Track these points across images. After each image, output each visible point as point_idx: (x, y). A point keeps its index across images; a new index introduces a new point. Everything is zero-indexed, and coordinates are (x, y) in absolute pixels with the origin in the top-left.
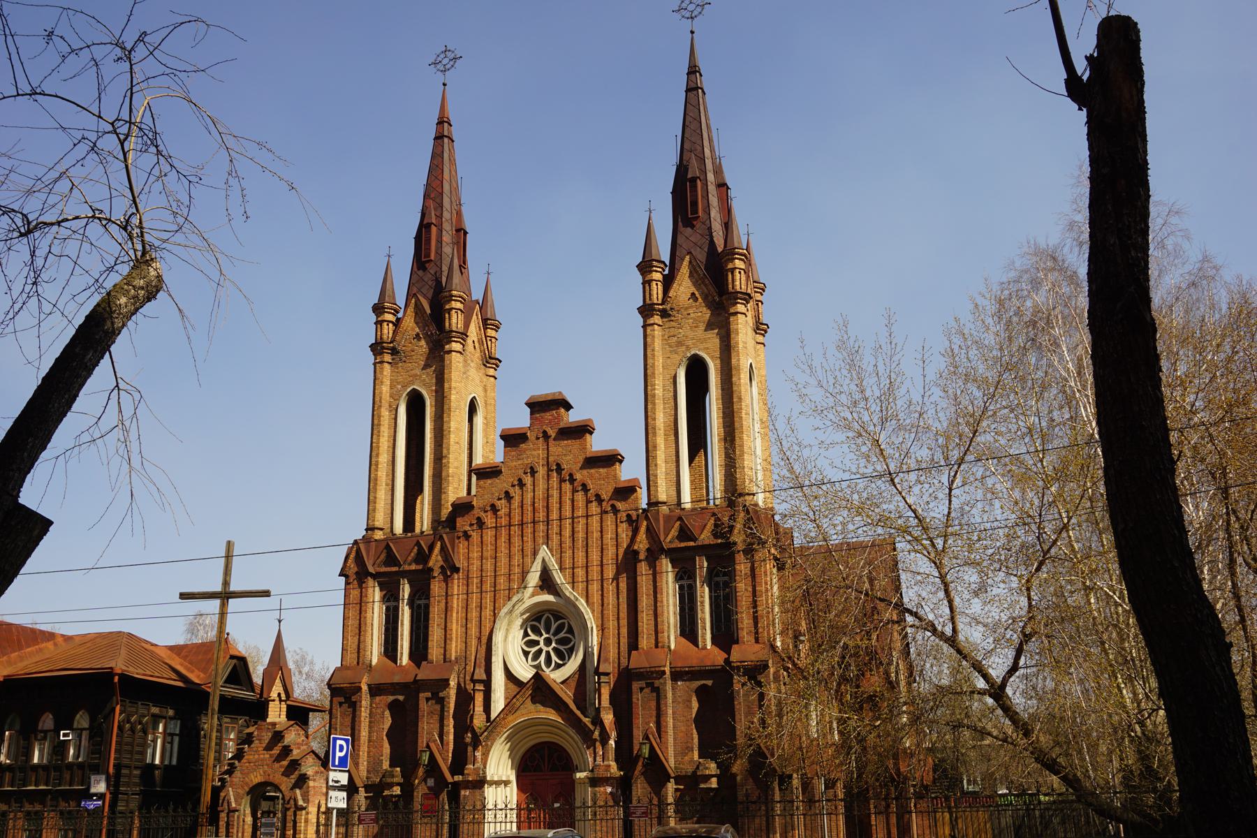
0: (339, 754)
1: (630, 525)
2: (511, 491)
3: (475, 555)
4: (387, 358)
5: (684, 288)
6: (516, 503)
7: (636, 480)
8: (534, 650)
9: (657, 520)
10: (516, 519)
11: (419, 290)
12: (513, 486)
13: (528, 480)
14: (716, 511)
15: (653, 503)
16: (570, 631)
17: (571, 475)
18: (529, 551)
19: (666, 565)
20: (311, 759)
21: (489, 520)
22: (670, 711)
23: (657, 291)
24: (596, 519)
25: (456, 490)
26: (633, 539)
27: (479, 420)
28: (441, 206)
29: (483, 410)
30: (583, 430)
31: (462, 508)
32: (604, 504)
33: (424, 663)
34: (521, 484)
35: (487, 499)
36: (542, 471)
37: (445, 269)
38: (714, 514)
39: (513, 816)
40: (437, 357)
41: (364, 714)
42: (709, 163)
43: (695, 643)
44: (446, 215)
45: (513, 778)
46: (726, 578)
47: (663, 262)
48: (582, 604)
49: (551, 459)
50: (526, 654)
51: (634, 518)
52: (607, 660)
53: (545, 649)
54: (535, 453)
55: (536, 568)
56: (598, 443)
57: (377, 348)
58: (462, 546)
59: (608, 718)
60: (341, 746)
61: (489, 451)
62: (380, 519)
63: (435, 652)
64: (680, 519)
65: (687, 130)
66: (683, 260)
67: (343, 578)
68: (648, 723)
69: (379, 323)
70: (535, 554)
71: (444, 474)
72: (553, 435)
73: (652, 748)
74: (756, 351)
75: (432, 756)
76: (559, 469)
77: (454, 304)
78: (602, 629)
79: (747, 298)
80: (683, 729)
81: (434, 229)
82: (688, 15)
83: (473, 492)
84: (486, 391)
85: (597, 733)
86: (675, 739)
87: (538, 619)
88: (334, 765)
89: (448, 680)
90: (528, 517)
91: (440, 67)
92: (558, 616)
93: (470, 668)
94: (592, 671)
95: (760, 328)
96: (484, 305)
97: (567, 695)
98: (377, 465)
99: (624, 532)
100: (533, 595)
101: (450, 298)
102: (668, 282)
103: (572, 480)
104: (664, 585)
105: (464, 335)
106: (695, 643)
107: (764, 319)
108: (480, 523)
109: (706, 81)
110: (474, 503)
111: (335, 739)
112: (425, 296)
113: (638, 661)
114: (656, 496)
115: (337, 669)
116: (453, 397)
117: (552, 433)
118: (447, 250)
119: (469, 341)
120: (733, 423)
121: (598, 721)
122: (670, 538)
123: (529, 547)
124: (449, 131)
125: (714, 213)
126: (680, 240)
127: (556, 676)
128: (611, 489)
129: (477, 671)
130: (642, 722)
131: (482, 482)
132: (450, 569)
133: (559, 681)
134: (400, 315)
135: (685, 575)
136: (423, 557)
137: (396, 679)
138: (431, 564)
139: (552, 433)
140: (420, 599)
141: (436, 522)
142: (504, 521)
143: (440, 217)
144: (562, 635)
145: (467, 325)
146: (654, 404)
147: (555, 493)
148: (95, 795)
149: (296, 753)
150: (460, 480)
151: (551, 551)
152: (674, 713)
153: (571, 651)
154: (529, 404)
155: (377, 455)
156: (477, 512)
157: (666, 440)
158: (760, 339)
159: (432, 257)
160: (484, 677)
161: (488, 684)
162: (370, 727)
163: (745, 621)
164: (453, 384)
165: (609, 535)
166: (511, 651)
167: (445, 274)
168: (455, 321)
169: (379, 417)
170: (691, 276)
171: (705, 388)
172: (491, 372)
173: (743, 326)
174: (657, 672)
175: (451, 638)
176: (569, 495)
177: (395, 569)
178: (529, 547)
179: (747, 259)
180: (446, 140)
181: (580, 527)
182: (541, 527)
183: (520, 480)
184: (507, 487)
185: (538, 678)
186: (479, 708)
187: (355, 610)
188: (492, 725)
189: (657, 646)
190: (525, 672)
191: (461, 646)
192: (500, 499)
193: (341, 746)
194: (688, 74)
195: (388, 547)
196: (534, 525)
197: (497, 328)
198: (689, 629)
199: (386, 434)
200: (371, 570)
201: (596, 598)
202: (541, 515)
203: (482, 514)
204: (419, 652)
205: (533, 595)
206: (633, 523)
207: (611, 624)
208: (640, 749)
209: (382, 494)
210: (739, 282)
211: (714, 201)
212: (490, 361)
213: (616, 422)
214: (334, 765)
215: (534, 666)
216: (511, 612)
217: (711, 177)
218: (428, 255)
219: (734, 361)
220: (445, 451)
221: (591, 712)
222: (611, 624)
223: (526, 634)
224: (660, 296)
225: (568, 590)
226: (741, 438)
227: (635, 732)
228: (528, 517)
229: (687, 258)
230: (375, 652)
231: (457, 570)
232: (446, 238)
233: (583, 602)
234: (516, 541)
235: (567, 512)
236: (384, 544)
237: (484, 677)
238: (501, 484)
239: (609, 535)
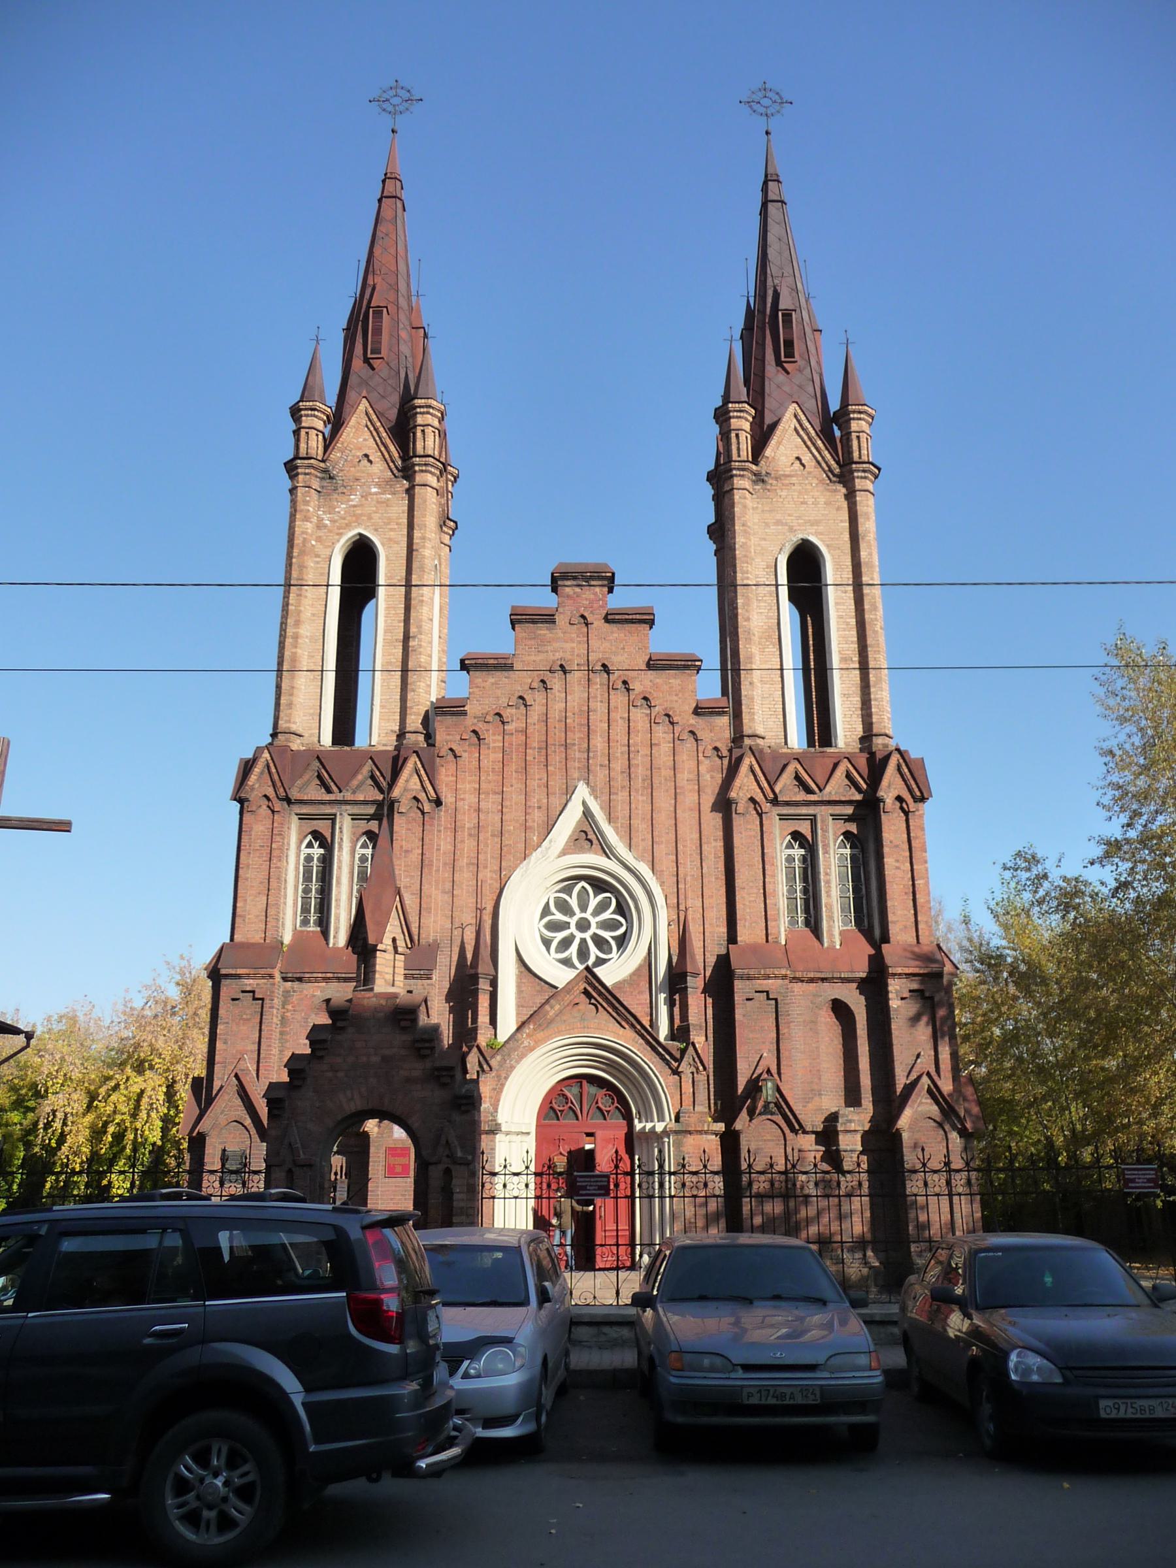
10: (535, 740)
23: (314, 444)
25: (430, 689)
31: (448, 709)
45: (533, 1130)
70: (569, 792)
82: (763, 110)
87: (568, 890)
100: (564, 853)
123: (557, 783)
151: (593, 792)
165: (685, 776)
178: (557, 783)
184: (520, 690)
196: (561, 755)
203: (480, 727)
205: (564, 853)
228: (557, 735)
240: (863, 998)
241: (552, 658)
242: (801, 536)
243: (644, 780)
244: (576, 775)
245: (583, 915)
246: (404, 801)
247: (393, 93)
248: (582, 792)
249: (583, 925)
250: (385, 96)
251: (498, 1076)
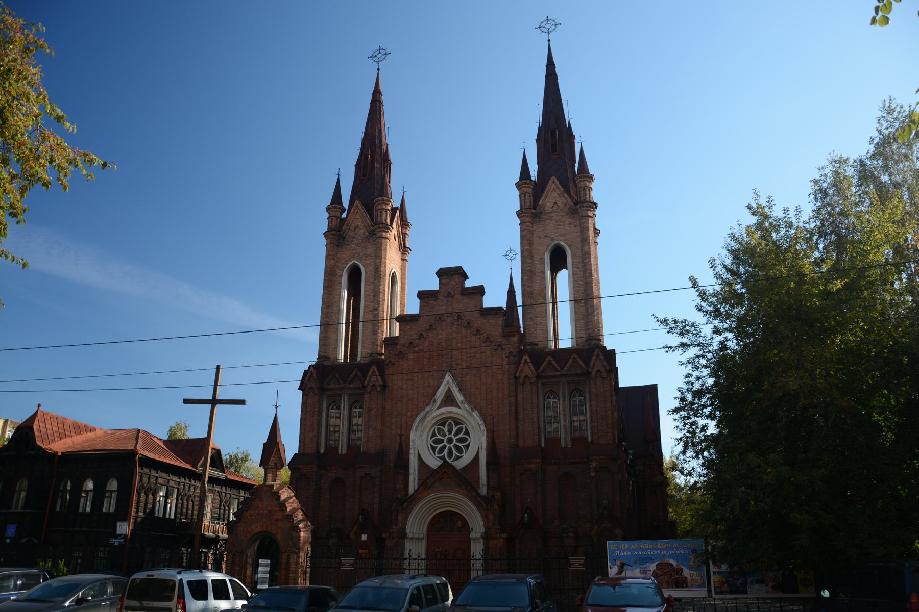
29: (407, 277)
39: (423, 564)
53: (445, 443)
61: (413, 307)
87: (443, 424)
109: (385, 99)
144: (461, 436)
148: (120, 535)
190: (433, 462)
205: (439, 407)
246: (594, 373)
248: (448, 378)
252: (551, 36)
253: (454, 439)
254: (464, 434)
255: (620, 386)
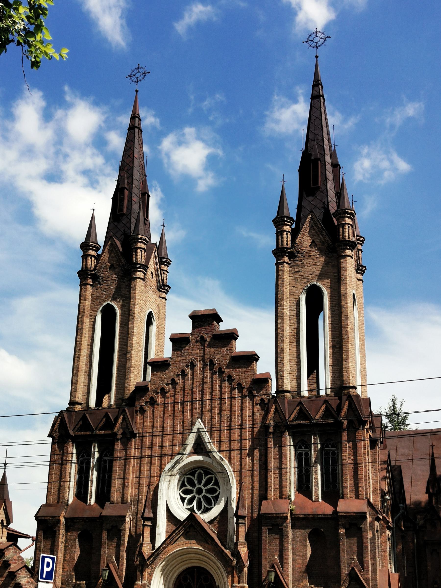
0: (46, 569)
1: (262, 408)
2: (177, 379)
3: (148, 424)
4: (90, 281)
5: (305, 240)
6: (179, 388)
7: (269, 374)
8: (189, 497)
9: (283, 404)
10: (180, 399)
11: (115, 234)
12: (178, 375)
13: (189, 371)
14: (327, 399)
15: (280, 391)
16: (217, 483)
17: (220, 369)
18: (188, 424)
19: (289, 441)
20: (24, 572)
21: (159, 400)
22: (290, 547)
23: (287, 239)
24: (238, 400)
25: (135, 378)
26: (265, 417)
27: (153, 328)
28: (131, 176)
30: (232, 336)
31: (141, 390)
32: (244, 390)
33: (107, 503)
34: (183, 374)
35: (159, 384)
36: (199, 365)
37: (133, 220)
38: (326, 402)
40: (125, 293)
41: (61, 539)
42: (327, 148)
43: (310, 498)
44: (135, 183)
46: (334, 449)
47: (292, 219)
48: (226, 463)
49: (206, 356)
50: (183, 499)
51: (266, 401)
52: (244, 506)
54: (194, 352)
55: (191, 439)
56: (241, 346)
57: (83, 274)
58: (139, 419)
59: (244, 551)
60: (48, 564)
62: (80, 397)
63: (115, 495)
64: (300, 403)
65: (311, 125)
66: (306, 217)
67: (51, 439)
68: (273, 556)
69: (85, 257)
70: (192, 424)
71: (128, 365)
72: (209, 340)
73: (277, 576)
74: (357, 285)
75: (111, 574)
76: (212, 363)
77: (139, 245)
78: (241, 483)
79: (353, 245)
80: (300, 561)
81: (126, 192)
82: (314, 45)
83: (149, 378)
84: (159, 308)
85: (235, 562)
86: (293, 569)
87: (193, 474)
88: (42, 578)
89: (124, 517)
90: (188, 397)
91: (134, 79)
92: (207, 471)
93: (141, 509)
94: (232, 515)
95: (360, 269)
96: (161, 247)
97: (212, 531)
98: (79, 357)
99: (258, 413)
101: (137, 240)
102: (295, 233)
103: (221, 372)
104: (288, 452)
105: (145, 267)
106: (310, 498)
107: (362, 262)
108: (153, 402)
109: (326, 93)
110: (149, 387)
111: (44, 558)
112: (118, 239)
113: (267, 508)
114: (283, 386)
115: (42, 506)
116: (136, 310)
117: (208, 338)
118: (135, 207)
119: (149, 272)
120: (341, 334)
121: (236, 554)
122: (291, 416)
123: (188, 419)
124: (140, 124)
125: (330, 185)
126: (305, 203)
127: (205, 517)
128: (249, 380)
129: (147, 511)
130: (269, 556)
131: (155, 373)
132: (129, 435)
133: (207, 520)
134: (100, 252)
135: (302, 446)
136: (109, 424)
137: (86, 515)
138: (116, 430)
139: (208, 338)
140: (106, 455)
141: (120, 399)
142: (170, 400)
143: (131, 183)
144: (210, 486)
145: (148, 260)
146: (283, 319)
147: (209, 381)
149: (13, 567)
150: (139, 370)
151: (204, 423)
152: (293, 549)
153: (216, 499)
154: (191, 317)
155: (80, 350)
156: (151, 394)
157: (291, 346)
158: (360, 277)
159: (125, 212)
160: (151, 515)
161: (154, 520)
162: (65, 550)
163: (349, 482)
164: (137, 301)
165: (247, 414)
166: (171, 498)
167: (133, 227)
168: (141, 257)
169: (82, 323)
170: (311, 227)
171: (321, 308)
172: (163, 295)
173: (349, 265)
174: (281, 517)
175: (128, 486)
176: (218, 382)
177: (88, 433)
178: (188, 419)
179: (352, 216)
180: (137, 130)
181: (226, 407)
182: (198, 405)
183: (183, 371)
184: (174, 376)
185: (192, 517)
186: (147, 539)
187: (58, 463)
188: (157, 553)
189: (281, 498)
190: (182, 513)
191: (135, 491)
192: (167, 385)
193: (48, 564)
194: (313, 86)
195: (84, 416)
196: (195, 403)
197: (168, 264)
198: (304, 487)
199: (87, 336)
200: (71, 433)
201: (236, 459)
202: (198, 397)
204: (103, 496)
206: (265, 406)
207: (247, 480)
208: (268, 576)
209: (82, 379)
210: (348, 234)
211: (330, 176)
212: (163, 287)
213: (255, 332)
214: (42, 578)
215: (188, 509)
216: (172, 468)
217: (328, 159)
218: (122, 210)
219: (343, 290)
220: (129, 349)
221: (229, 544)
222: (247, 480)
223: (183, 485)
224: (289, 243)
225: (217, 455)
226: (347, 346)
227: (264, 562)
228: (188, 397)
229: (310, 216)
230: (71, 496)
231: (134, 435)
232: (135, 199)
233: (227, 461)
234: (179, 415)
235: (217, 395)
236: (82, 415)
237: (151, 515)
238: (171, 373)
239: (247, 414)
240: (11, 500)
241: (188, 358)
242: (312, 283)
243: (228, 417)
244: (197, 416)
245: (200, 486)
247: (136, 71)
249: (199, 491)
250: (134, 73)
251: (152, 567)
252: (321, 52)
253: (204, 489)
254: (185, 498)
255: (19, 539)
